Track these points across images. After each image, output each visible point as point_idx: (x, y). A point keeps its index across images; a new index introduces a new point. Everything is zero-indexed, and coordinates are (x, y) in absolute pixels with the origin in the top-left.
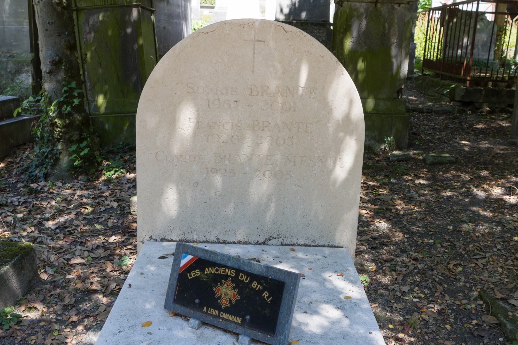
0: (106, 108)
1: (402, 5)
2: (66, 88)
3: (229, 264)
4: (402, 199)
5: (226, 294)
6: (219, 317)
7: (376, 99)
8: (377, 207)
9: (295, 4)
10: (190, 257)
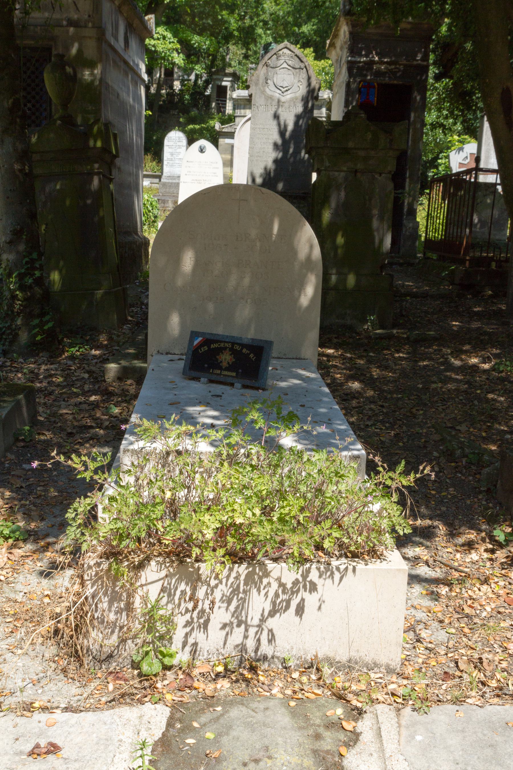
0: (63, 285)
1: (383, 175)
2: (27, 259)
3: (227, 340)
4: (378, 367)
5: (225, 359)
6: (221, 374)
7: (358, 275)
8: (352, 372)
9: (270, 172)
10: (200, 339)
